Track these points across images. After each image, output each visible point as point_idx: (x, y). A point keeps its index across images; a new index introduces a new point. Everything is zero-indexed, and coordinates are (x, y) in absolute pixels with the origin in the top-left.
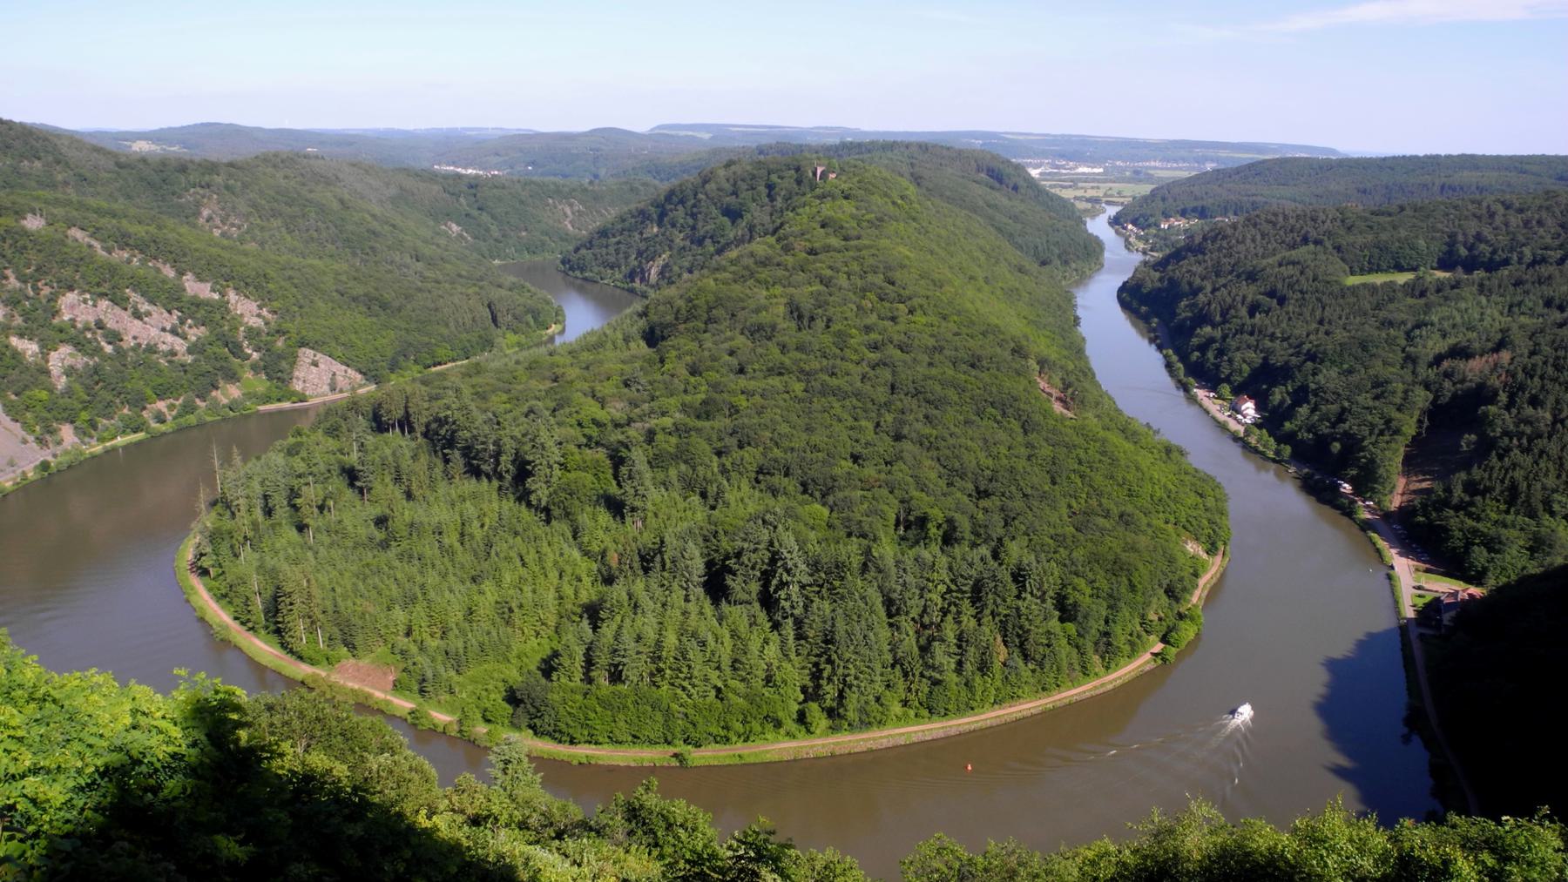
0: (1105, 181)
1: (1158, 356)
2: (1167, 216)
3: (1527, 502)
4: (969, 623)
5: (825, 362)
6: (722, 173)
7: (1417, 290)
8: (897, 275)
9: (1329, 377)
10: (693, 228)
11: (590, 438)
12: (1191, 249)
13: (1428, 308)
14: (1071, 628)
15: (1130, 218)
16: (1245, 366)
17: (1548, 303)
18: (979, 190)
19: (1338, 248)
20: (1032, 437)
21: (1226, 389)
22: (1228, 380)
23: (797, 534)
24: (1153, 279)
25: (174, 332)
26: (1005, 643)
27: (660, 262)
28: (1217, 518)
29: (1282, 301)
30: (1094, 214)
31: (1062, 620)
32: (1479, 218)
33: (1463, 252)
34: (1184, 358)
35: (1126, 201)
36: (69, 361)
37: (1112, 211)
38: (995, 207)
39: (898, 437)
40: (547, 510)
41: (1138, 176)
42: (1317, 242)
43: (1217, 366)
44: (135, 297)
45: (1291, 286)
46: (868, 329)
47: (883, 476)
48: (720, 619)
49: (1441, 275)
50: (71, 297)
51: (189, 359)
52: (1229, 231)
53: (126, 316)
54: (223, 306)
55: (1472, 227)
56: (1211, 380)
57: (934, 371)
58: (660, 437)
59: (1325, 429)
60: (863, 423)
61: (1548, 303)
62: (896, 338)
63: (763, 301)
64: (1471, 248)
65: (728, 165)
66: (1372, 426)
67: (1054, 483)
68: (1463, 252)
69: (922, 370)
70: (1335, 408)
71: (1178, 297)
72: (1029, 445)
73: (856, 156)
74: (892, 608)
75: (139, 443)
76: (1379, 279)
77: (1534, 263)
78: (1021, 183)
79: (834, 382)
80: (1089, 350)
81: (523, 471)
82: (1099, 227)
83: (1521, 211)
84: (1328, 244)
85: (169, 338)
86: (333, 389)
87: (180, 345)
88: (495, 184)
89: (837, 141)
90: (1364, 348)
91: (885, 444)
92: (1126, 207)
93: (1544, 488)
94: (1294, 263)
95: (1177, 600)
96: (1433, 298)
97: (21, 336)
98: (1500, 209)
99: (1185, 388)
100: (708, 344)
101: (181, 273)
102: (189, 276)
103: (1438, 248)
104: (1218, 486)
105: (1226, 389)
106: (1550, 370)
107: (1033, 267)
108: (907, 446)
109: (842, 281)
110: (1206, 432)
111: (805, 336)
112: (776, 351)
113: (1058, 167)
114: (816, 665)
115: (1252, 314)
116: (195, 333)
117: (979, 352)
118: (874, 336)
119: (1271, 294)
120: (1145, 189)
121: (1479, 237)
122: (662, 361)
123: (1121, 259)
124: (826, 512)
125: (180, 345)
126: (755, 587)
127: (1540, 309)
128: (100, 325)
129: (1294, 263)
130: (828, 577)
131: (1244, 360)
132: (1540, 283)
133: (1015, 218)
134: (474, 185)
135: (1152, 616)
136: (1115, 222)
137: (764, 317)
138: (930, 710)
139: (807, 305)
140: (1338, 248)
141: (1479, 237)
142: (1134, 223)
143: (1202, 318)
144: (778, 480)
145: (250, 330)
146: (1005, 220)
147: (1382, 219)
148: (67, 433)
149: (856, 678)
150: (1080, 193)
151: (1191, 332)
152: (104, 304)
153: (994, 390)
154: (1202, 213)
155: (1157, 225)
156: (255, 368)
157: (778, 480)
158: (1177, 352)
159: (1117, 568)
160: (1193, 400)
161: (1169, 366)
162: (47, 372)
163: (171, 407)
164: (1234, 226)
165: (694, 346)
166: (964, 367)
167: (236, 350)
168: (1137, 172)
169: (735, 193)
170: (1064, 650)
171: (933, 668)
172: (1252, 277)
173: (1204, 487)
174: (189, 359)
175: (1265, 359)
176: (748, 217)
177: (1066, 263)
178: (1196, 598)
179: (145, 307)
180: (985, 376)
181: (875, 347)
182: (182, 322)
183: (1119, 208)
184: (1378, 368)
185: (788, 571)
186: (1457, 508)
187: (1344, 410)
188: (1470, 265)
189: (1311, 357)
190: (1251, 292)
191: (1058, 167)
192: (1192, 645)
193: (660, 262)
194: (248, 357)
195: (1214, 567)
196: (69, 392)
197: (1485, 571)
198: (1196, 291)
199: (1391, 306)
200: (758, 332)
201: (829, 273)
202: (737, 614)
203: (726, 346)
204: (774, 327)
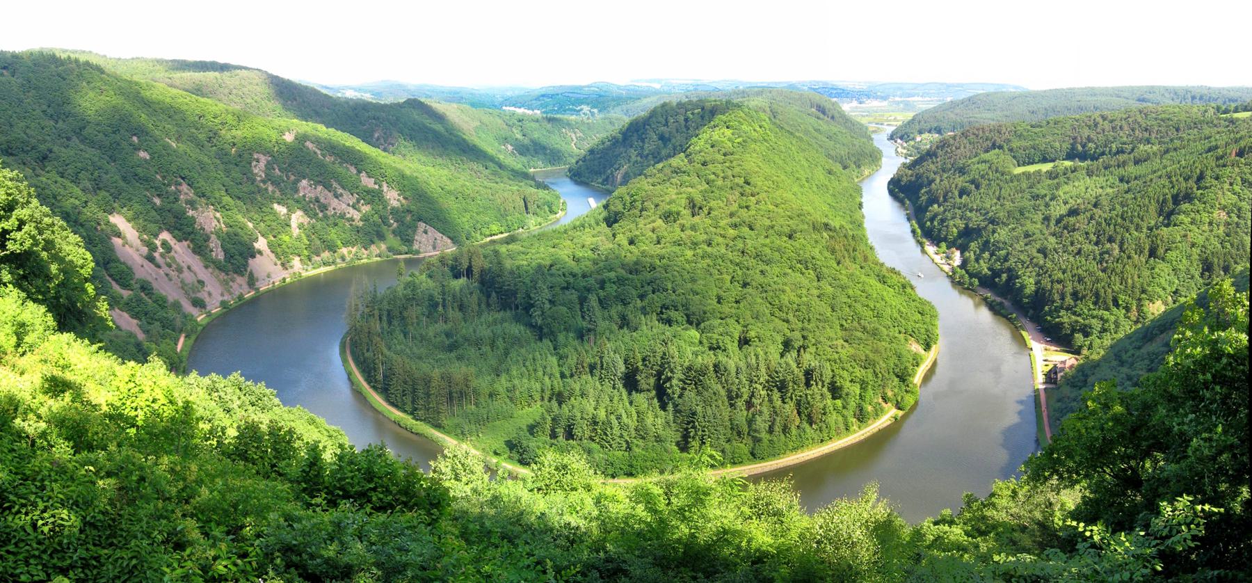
1: (908, 225)
2: (920, 132)
3: (1105, 302)
4: (778, 403)
7: (1052, 175)
9: (1002, 234)
10: (642, 148)
11: (569, 283)
12: (930, 154)
13: (1058, 187)
14: (839, 402)
15: (900, 135)
16: (955, 230)
17: (1121, 180)
18: (813, 120)
19: (1011, 150)
20: (821, 284)
21: (943, 245)
22: (945, 240)
23: (679, 347)
24: (909, 175)
25: (354, 207)
26: (799, 413)
27: (623, 170)
28: (930, 327)
29: (977, 187)
31: (834, 398)
32: (1089, 127)
33: (1080, 148)
34: (922, 226)
36: (301, 220)
37: (890, 130)
38: (817, 130)
39: (745, 285)
40: (541, 328)
41: (908, 106)
42: (1000, 147)
43: (940, 230)
44: (335, 185)
45: (983, 177)
47: (733, 311)
48: (631, 403)
49: (1068, 163)
50: (304, 182)
51: (361, 224)
52: (952, 141)
53: (330, 195)
55: (1086, 132)
56: (936, 240)
57: (768, 241)
58: (607, 285)
59: (998, 266)
60: (725, 276)
61: (1121, 180)
63: (674, 197)
64: (1084, 146)
66: (1023, 263)
67: (833, 310)
68: (1080, 148)
69: (762, 240)
70: (1003, 252)
71: (921, 186)
74: (732, 398)
76: (1031, 169)
77: (1118, 152)
78: (836, 115)
79: (709, 249)
80: (867, 225)
81: (528, 307)
83: (1111, 121)
84: (1006, 147)
85: (351, 210)
90: (1022, 214)
91: (736, 290)
93: (1113, 291)
94: (985, 162)
96: (1062, 179)
97: (279, 203)
98: (1101, 121)
99: (921, 244)
100: (641, 226)
101: (359, 172)
102: (364, 174)
103: (1066, 146)
104: (933, 307)
105: (943, 245)
106: (1119, 220)
107: (838, 168)
108: (749, 290)
109: (720, 182)
110: (928, 271)
111: (697, 219)
114: (686, 429)
115: (961, 197)
116: (366, 209)
118: (735, 220)
119: (972, 182)
120: (909, 115)
121: (1089, 139)
122: (614, 235)
123: (892, 162)
124: (698, 335)
125: (357, 216)
126: (652, 381)
127: (1117, 182)
128: (317, 200)
129: (985, 162)
130: (695, 377)
131: (955, 227)
132: (1119, 166)
133: (829, 138)
135: (890, 394)
136: (892, 137)
137: (674, 208)
138: (754, 456)
139: (698, 199)
140: (1011, 150)
141: (1089, 139)
142: (901, 138)
143: (933, 200)
144: (673, 314)
145: (393, 208)
147: (1037, 130)
148: (296, 262)
151: (925, 210)
152: (320, 188)
154: (939, 131)
155: (914, 139)
156: (394, 232)
157: (673, 314)
158: (918, 223)
160: (923, 251)
161: (913, 232)
162: (289, 226)
163: (350, 252)
164: (954, 138)
165: (633, 226)
166: (785, 239)
167: (384, 220)
169: (666, 125)
170: (833, 418)
171: (755, 431)
172: (962, 171)
173: (925, 311)
174: (361, 224)
175: (967, 225)
176: (673, 140)
177: (859, 167)
178: (917, 379)
179: (340, 191)
181: (735, 226)
182: (358, 201)
184: (1029, 227)
185: (672, 371)
186: (1067, 309)
187: (1008, 254)
188: (1083, 157)
189: (992, 221)
190: (960, 181)
192: (913, 408)
193: (623, 170)
194: (390, 226)
195: (928, 359)
196: (299, 239)
197: (1081, 347)
198: (931, 182)
199: (1039, 186)
200: (668, 217)
201: (713, 177)
202: (640, 398)
203: (650, 226)
204: (678, 214)
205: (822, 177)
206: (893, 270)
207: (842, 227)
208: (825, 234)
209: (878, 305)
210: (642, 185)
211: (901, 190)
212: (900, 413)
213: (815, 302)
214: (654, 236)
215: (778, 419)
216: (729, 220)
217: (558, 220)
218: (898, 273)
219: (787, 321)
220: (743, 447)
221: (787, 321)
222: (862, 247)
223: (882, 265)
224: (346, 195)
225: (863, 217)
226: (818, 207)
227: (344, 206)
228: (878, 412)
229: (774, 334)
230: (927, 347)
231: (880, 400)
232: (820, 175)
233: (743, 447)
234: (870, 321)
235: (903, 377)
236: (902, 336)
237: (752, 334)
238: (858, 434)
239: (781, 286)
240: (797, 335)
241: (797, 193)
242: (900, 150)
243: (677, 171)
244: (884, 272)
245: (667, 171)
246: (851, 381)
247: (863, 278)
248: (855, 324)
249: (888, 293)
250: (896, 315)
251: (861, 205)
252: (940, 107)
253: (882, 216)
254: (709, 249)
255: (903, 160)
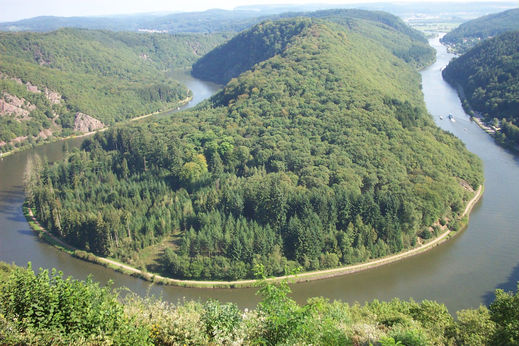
0: (440, 22)
5: (300, 110)
6: (261, 27)
8: (334, 69)
12: (476, 51)
30: (432, 36)
35: (448, 31)
37: (442, 36)
46: (320, 95)
52: (491, 42)
54: (42, 97)
57: (349, 112)
62: (332, 97)
65: (263, 23)
72: (390, 144)
73: (77, 32)
75: (10, 156)
78: (399, 25)
80: (426, 99)
82: (434, 43)
86: (90, 130)
87: (26, 113)
88: (163, 36)
89: (75, 26)
92: (448, 34)
95: (210, 181)
112: (280, 106)
113: (417, 17)
117: (369, 103)
118: (323, 98)
120: (457, 25)
134: (153, 38)
136: (444, 41)
138: (343, 261)
146: (390, 42)
149: (308, 247)
150: (427, 28)
153: (375, 119)
154: (479, 35)
159: (427, 197)
164: (493, 40)
168: (454, 17)
180: (371, 114)
183: (446, 34)
191: (417, 17)
194: (54, 117)
203: (258, 104)
205: (389, 67)
206: (447, 133)
207: (406, 102)
208: (393, 107)
209: (436, 156)
210: (249, 77)
211: (453, 76)
212: (453, 233)
213: (386, 153)
214: (261, 111)
215: (360, 235)
216: (318, 98)
217: (187, 103)
218: (452, 135)
219: (367, 167)
220: (335, 257)
221: (367, 167)
222: (423, 116)
223: (439, 129)
224: (15, 99)
225: (423, 94)
226: (390, 88)
227: (15, 108)
228: (436, 232)
229: (357, 176)
230: (475, 187)
231: (438, 224)
232: (387, 65)
233: (335, 257)
234: (430, 168)
235: (455, 208)
236: (454, 178)
237: (340, 175)
238: (423, 247)
239: (360, 142)
240: (374, 176)
241: (373, 74)
242: (450, 49)
243: (276, 66)
244: (441, 134)
245: (269, 67)
246: (416, 209)
247: (424, 137)
248: (418, 169)
249: (444, 148)
250: (450, 163)
251: (420, 87)
252: (481, 18)
253: (440, 101)
254: (304, 118)
255: (453, 56)
